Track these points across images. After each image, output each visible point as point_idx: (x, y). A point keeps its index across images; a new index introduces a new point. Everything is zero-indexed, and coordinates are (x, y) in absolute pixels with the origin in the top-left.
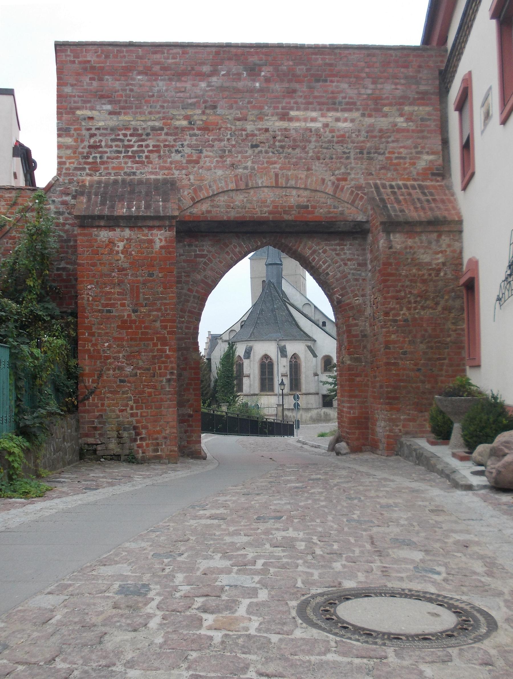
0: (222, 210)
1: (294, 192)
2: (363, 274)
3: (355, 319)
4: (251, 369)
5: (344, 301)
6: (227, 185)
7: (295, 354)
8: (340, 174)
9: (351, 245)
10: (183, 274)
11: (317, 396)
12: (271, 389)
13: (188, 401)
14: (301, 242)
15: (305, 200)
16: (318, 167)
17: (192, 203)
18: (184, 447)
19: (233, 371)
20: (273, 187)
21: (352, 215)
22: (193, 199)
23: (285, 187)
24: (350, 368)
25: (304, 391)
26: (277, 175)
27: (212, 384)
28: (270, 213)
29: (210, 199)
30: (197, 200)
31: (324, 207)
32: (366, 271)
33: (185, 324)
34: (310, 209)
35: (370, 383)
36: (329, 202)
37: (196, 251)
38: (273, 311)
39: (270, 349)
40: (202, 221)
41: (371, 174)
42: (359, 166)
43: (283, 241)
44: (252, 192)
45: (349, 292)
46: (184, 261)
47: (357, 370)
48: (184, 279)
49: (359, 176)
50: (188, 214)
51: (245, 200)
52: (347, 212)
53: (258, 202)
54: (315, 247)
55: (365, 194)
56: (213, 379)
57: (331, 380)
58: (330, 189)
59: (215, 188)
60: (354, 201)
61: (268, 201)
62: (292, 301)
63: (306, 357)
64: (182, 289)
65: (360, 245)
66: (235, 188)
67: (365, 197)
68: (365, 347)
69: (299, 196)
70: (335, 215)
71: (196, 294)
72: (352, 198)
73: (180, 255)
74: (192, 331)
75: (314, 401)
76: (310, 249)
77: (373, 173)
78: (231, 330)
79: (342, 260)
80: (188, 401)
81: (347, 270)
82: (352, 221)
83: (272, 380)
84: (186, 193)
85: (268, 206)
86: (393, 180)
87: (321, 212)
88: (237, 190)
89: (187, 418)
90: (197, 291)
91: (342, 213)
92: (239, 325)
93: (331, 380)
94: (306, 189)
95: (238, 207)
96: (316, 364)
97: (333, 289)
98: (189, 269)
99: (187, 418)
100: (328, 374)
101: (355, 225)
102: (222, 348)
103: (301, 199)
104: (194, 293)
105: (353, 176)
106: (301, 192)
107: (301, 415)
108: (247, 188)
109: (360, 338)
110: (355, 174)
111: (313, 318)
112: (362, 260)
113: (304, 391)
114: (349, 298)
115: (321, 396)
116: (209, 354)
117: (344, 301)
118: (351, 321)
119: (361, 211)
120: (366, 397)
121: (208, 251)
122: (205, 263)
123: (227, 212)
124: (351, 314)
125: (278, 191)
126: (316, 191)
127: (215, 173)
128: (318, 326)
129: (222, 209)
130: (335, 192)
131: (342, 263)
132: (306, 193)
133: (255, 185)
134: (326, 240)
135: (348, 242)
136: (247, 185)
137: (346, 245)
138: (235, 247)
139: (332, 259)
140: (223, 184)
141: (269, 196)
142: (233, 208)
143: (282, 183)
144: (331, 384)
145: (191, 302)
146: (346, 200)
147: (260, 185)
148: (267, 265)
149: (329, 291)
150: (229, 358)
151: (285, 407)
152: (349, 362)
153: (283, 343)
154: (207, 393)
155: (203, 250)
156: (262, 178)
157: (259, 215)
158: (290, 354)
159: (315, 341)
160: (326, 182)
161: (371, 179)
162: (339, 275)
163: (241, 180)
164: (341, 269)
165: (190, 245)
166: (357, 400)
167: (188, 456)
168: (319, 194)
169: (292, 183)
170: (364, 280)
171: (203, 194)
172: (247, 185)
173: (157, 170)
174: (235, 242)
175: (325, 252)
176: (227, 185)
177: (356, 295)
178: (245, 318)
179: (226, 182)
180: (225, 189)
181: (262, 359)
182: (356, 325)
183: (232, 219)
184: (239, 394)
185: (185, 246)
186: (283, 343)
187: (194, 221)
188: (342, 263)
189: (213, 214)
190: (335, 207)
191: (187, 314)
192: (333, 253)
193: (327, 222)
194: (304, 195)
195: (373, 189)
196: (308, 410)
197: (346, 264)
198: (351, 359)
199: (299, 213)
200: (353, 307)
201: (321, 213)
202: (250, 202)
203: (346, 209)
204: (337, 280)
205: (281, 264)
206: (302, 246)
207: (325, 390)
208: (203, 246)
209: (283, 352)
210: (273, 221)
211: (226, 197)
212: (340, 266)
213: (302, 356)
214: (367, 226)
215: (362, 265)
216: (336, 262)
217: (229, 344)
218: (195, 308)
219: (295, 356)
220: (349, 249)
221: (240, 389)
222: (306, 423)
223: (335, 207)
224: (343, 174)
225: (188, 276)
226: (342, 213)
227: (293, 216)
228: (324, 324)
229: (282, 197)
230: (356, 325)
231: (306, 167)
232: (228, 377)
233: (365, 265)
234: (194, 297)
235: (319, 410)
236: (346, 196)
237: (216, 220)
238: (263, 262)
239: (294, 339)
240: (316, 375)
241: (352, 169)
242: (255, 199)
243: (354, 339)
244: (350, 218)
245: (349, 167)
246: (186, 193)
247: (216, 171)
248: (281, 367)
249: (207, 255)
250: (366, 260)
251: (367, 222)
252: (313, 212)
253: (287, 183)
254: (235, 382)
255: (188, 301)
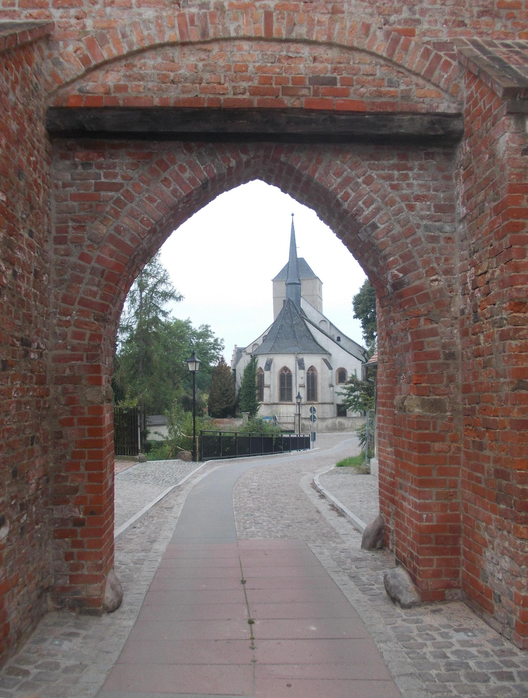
0: (150, 85)
1: (306, 51)
2: (447, 228)
3: (431, 321)
4: (271, 380)
5: (408, 284)
6: (161, 32)
7: (312, 366)
8: (399, 23)
9: (421, 168)
10: (70, 224)
11: (332, 406)
12: (290, 399)
13: (76, 490)
14: (319, 162)
15: (329, 66)
16: (356, 6)
17: (83, 69)
18: (64, 589)
19: (254, 381)
20: (259, 39)
21: (427, 100)
22: (85, 60)
23: (287, 41)
24: (420, 423)
25: (320, 401)
26: (268, 16)
27: (237, 393)
28: (254, 92)
29: (124, 62)
30: (94, 63)
31: (368, 85)
32: (453, 221)
33: (72, 328)
34: (339, 86)
35: (462, 455)
36: (379, 72)
37: (98, 176)
38: (292, 326)
39: (287, 361)
40: (106, 108)
41: (462, 24)
42: (438, 6)
43: (283, 158)
44: (215, 48)
45: (419, 264)
46: (73, 197)
47: (434, 429)
48: (71, 234)
49: (439, 26)
50: (75, 92)
51: (200, 65)
52: (415, 93)
53: (229, 69)
54: (348, 172)
55: (452, 57)
56: (237, 388)
57: (345, 391)
58: (381, 46)
59: (134, 38)
60: (431, 71)
61: (251, 68)
62: (309, 318)
63: (322, 370)
64: (68, 254)
65: (441, 169)
66: (177, 38)
67: (454, 63)
68: (451, 379)
69: (315, 59)
70: (391, 100)
71: (97, 265)
72: (427, 64)
73: (65, 186)
74: (86, 342)
75: (330, 411)
76: (338, 174)
77: (467, 21)
78: (254, 344)
79: (405, 198)
80: (76, 490)
81: (414, 220)
82: (427, 114)
83: (290, 390)
84: (71, 49)
85: (250, 79)
86: (507, 35)
87: (361, 95)
88: (184, 44)
89: (70, 526)
90: (100, 260)
91: (406, 96)
92: (261, 340)
93: (345, 391)
94: (330, 45)
95: (186, 79)
96: (333, 375)
97: (385, 258)
98: (82, 213)
99: (70, 526)
100: (343, 385)
101: (432, 123)
102: (245, 360)
103: (319, 66)
104: (93, 264)
105: (425, 26)
106: (320, 51)
107: (317, 424)
108: (206, 41)
109: (441, 361)
110: (430, 22)
111: (328, 334)
112: (445, 200)
113: (320, 401)
114: (419, 277)
115: (335, 405)
116: (235, 365)
117: (408, 284)
118: (423, 325)
119: (446, 91)
120: (454, 485)
121: (124, 178)
122: (118, 202)
123: (160, 89)
124: (423, 310)
125: (273, 49)
126: (352, 49)
127: (140, 14)
128: (333, 340)
129: (151, 83)
130: (392, 49)
131: (403, 205)
132: (333, 54)
133: (221, 35)
134: (372, 157)
135: (416, 163)
136: (204, 33)
137: (411, 169)
138: (182, 169)
139: (383, 197)
140: (153, 31)
141: (252, 57)
142: (173, 82)
143: (279, 31)
144: (345, 395)
145: (85, 281)
146: (414, 68)
147: (233, 34)
148: (287, 284)
149: (376, 264)
150: (251, 368)
151: (303, 416)
152: (417, 410)
153: (300, 357)
154: (231, 401)
155: (115, 176)
156: (236, 19)
157: (231, 96)
158: (307, 366)
159: (331, 355)
160: (372, 30)
161: (462, 34)
162: (397, 229)
163: (192, 22)
164: (402, 216)
165: (86, 165)
166: (434, 490)
167: (72, 608)
168: (358, 56)
169: (301, 31)
170: (449, 239)
171: (109, 51)
172: (204, 33)
173: (16, 8)
174: (182, 158)
175: (369, 181)
176: (161, 32)
177: (432, 271)
178: (266, 334)
179: (159, 25)
180: (157, 41)
181: (281, 371)
182: (434, 333)
183: (172, 104)
184: (260, 403)
185: (75, 166)
186: (300, 357)
187: (88, 109)
188: (403, 205)
189: (131, 93)
190: (391, 84)
191: (77, 306)
192: (386, 184)
193: (376, 114)
194: (325, 56)
195: (471, 47)
196: (323, 419)
197: (411, 208)
198: (423, 405)
199: (316, 93)
200: (427, 295)
201: (362, 95)
202: (212, 69)
203: (414, 87)
204: (394, 239)
205: (300, 284)
206: (321, 169)
207: (340, 400)
208: (114, 166)
209: (301, 364)
210: (260, 110)
211: (159, 60)
212: (400, 211)
213: (318, 369)
214: (457, 125)
215: (446, 209)
216: (392, 203)
217: (252, 357)
218: (94, 294)
219: (312, 368)
220: (418, 177)
221: (261, 398)
222: (321, 431)
223: (391, 84)
224: (406, 21)
225: (82, 228)
226: (406, 96)
227: (303, 99)
228: (339, 339)
229: (279, 61)
230: (434, 333)
231: (330, 6)
232: (250, 387)
233: (452, 208)
234: (93, 271)
235: (334, 420)
236: (413, 60)
237: (137, 105)
238: (283, 284)
239: (311, 352)
240: (331, 386)
241: (423, 12)
242: (221, 63)
243: (429, 362)
244: (423, 108)
245: (417, 8)
246: (71, 49)
247: (142, 10)
248: (300, 378)
249: (122, 185)
250: (451, 199)
251: (458, 115)
252: (345, 93)
253: (290, 31)
254: (257, 392)
255: (80, 280)
